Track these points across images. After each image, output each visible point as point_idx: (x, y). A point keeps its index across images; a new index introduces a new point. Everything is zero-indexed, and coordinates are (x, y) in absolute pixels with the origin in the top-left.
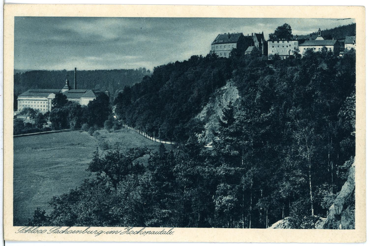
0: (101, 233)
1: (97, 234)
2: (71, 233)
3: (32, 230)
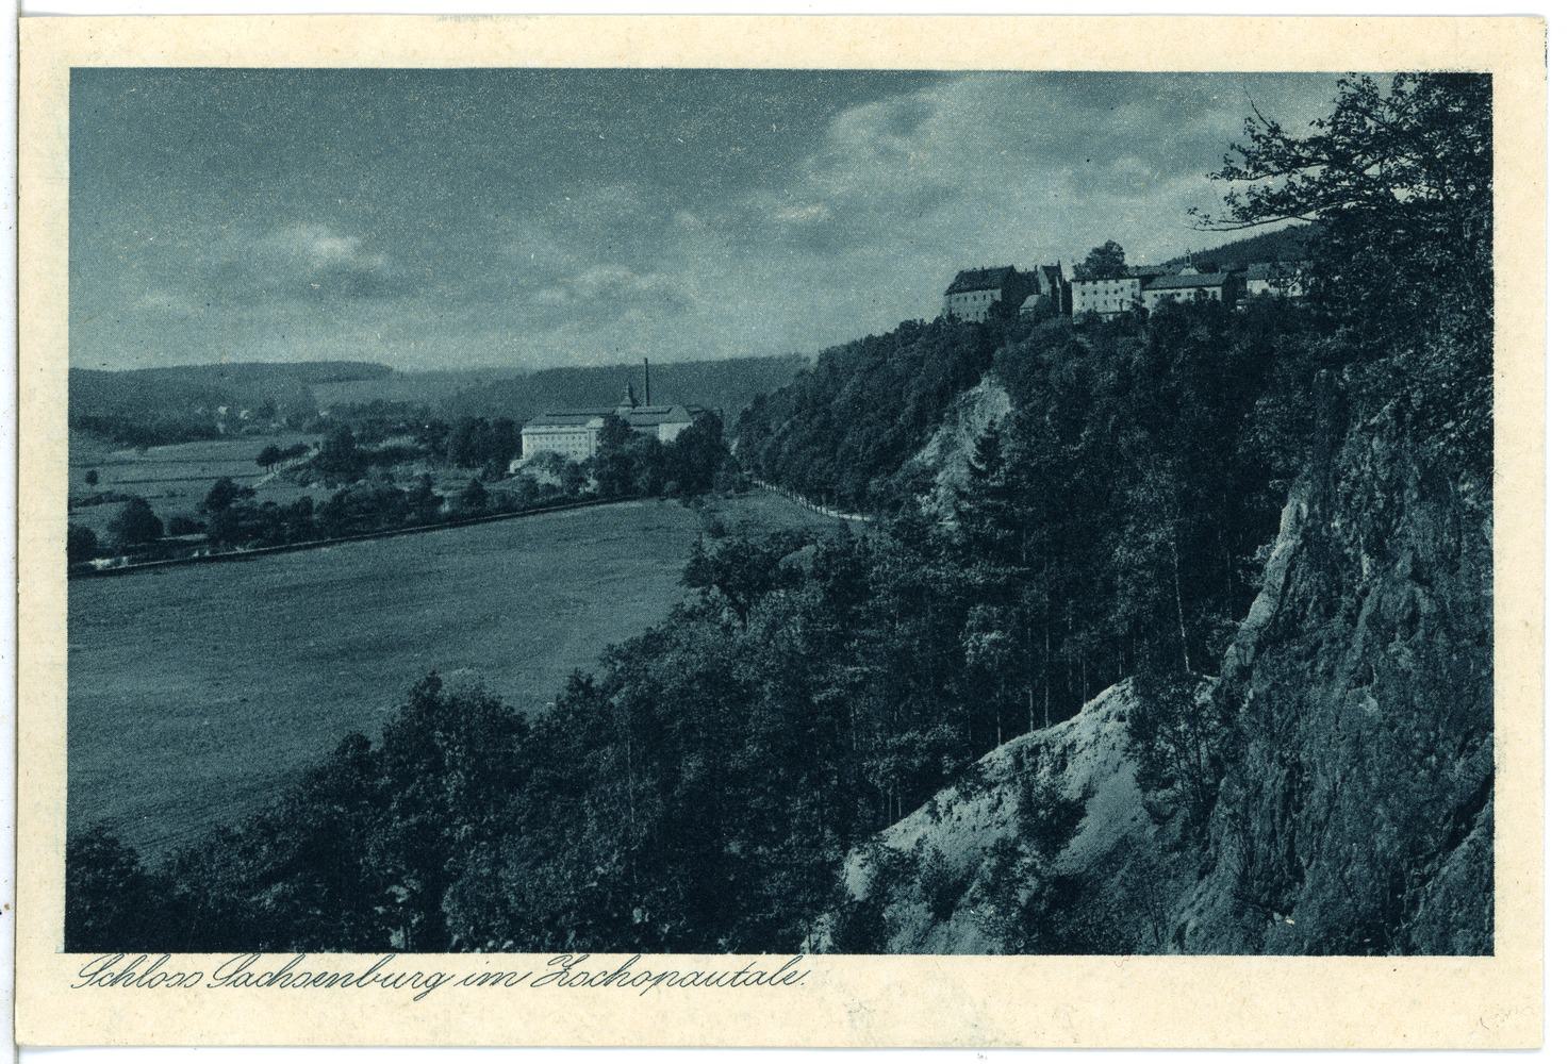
0: (434, 986)
1: (423, 989)
2: (304, 984)
3: (139, 971)
